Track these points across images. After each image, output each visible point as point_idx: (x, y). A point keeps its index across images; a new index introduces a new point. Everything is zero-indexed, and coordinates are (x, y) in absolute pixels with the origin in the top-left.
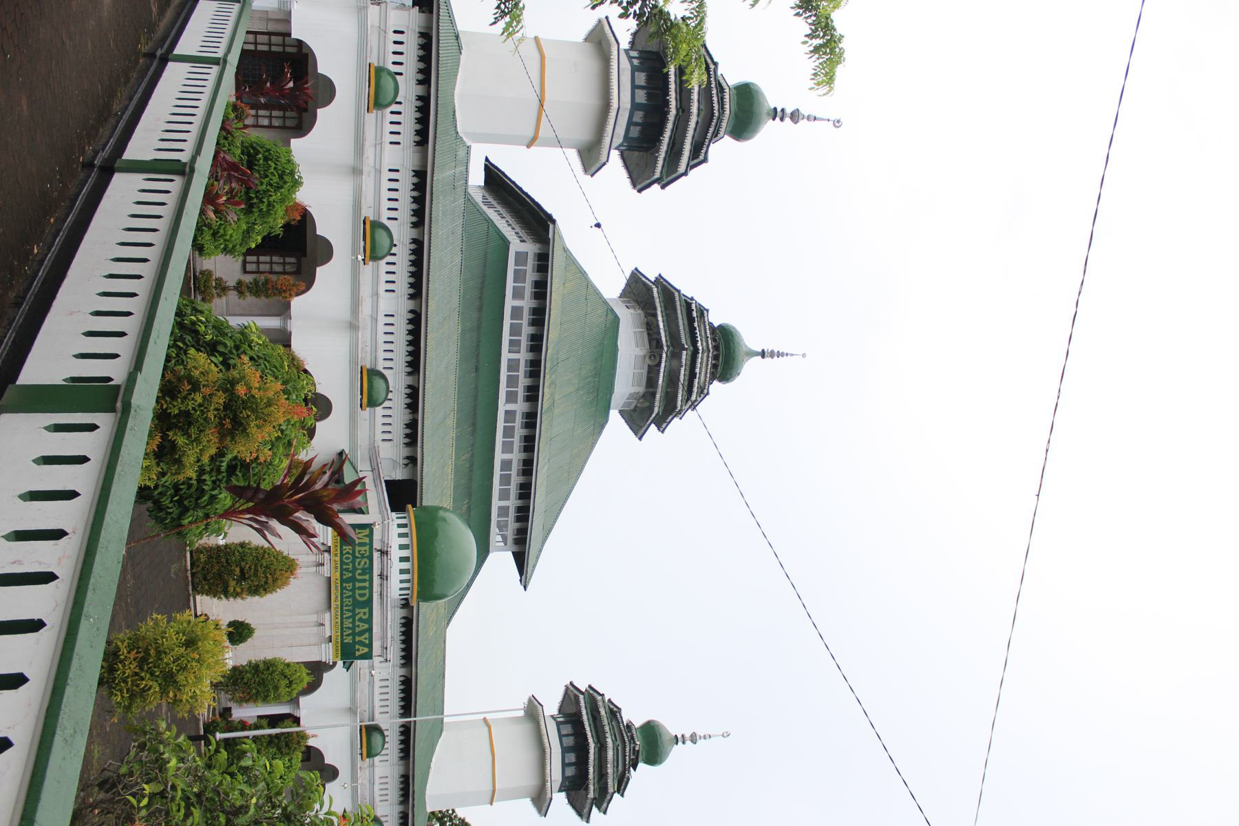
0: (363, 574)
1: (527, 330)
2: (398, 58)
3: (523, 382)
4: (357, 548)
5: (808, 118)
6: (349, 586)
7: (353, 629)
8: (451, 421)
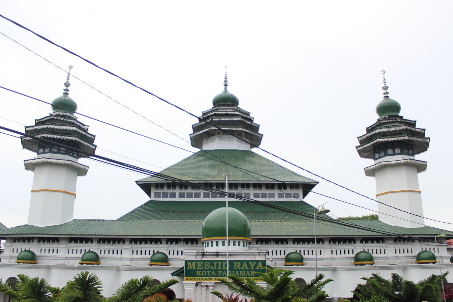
0: (213, 265)
2: (148, 252)
3: (165, 190)
4: (198, 268)
5: (385, 83)
7: (246, 271)
8: (166, 222)
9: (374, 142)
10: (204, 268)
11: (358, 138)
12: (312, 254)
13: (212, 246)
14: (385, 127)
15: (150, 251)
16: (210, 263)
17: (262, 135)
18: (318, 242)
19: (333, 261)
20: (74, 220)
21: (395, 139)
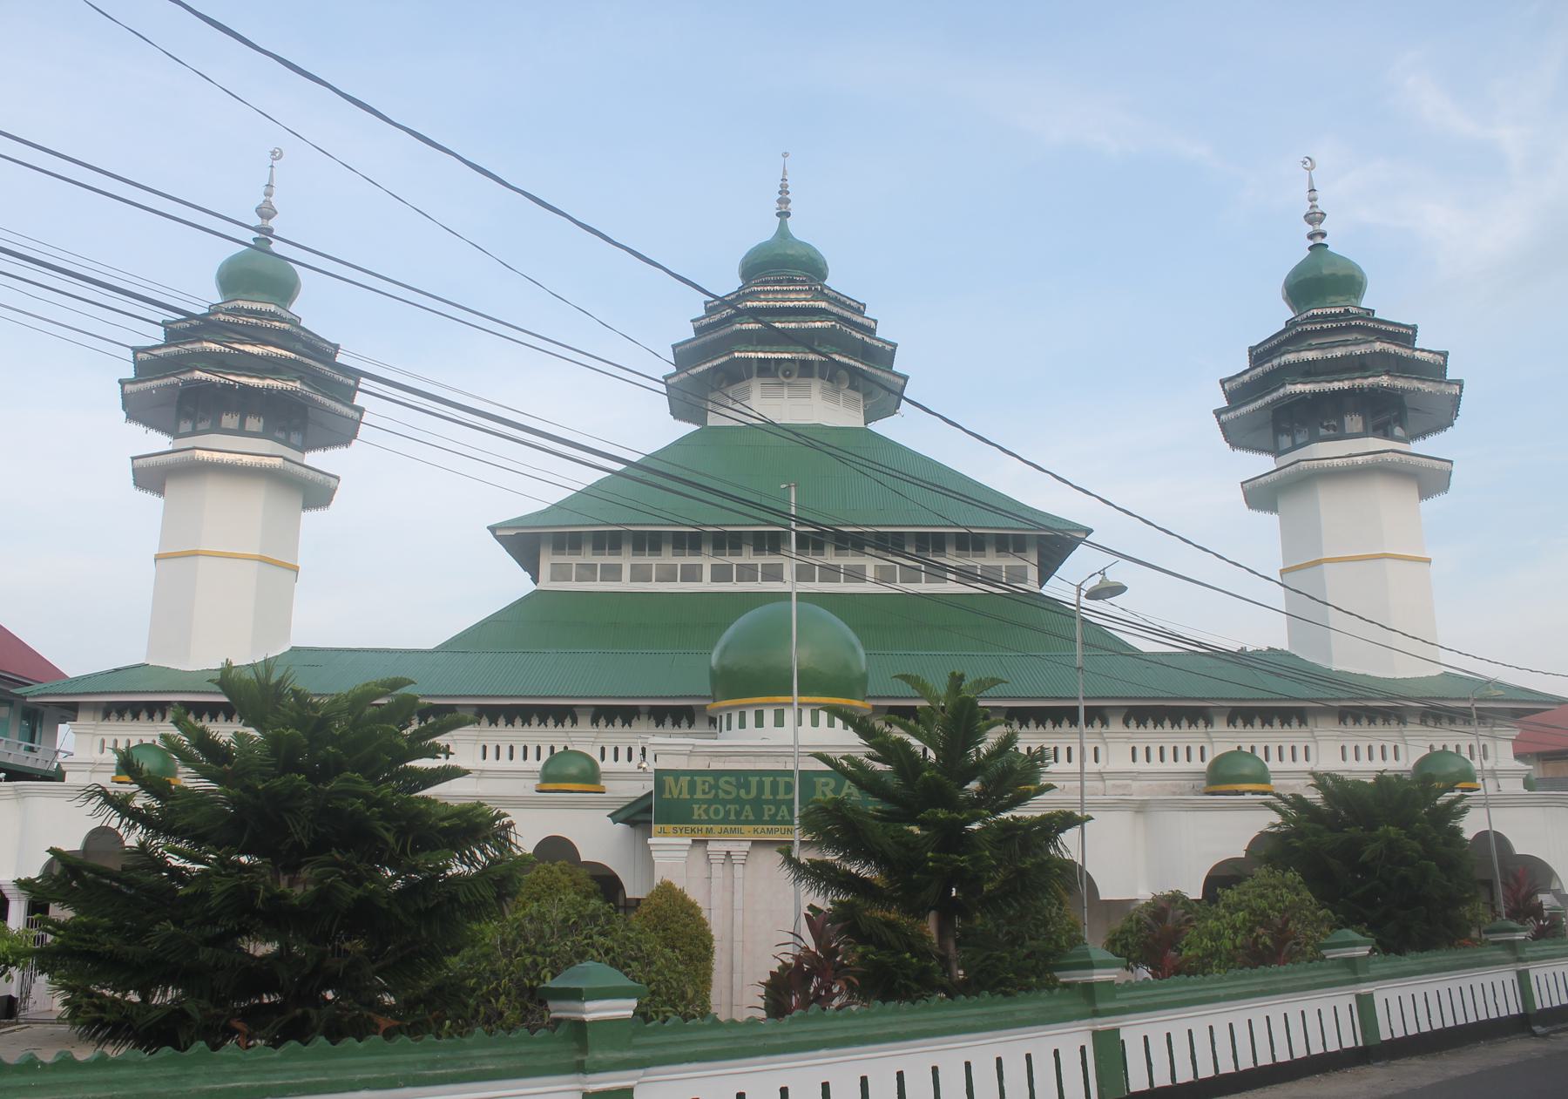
0: (747, 787)
2: (532, 753)
3: (748, 557)
4: (699, 795)
6: (768, 810)
9: (1275, 395)
10: (716, 795)
11: (1222, 382)
12: (1069, 760)
15: (539, 748)
16: (738, 780)
17: (906, 378)
18: (1089, 722)
20: (293, 649)
21: (1346, 385)
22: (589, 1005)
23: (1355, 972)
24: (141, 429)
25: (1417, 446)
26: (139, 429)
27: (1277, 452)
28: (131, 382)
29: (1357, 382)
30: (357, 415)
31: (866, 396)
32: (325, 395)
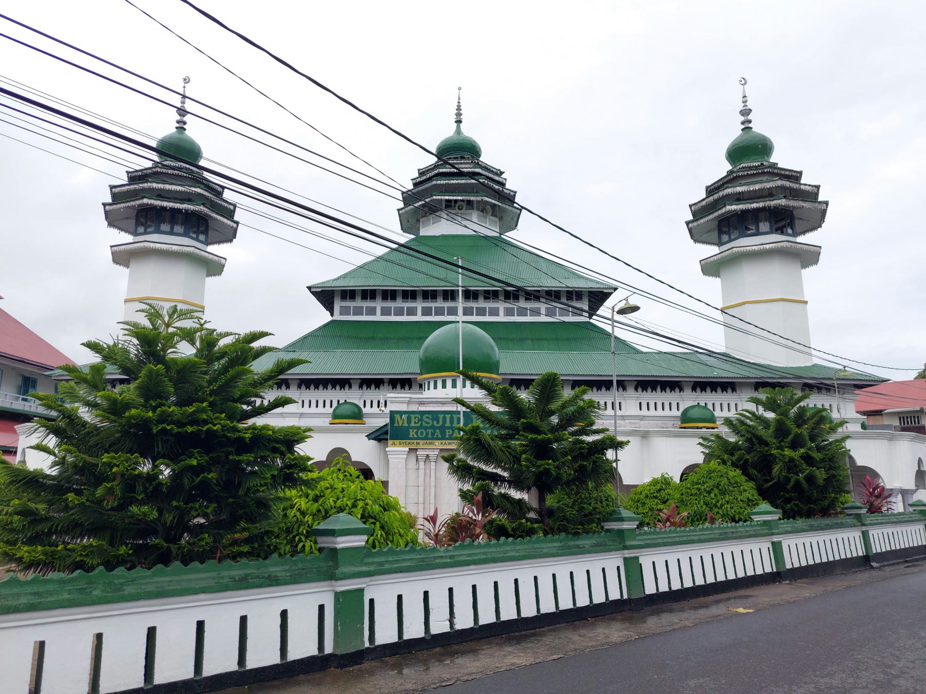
1: (399, 303)
2: (328, 404)
4: (413, 424)
5: (745, 102)
9: (720, 212)
11: (690, 206)
13: (435, 387)
14: (741, 185)
19: (642, 422)
21: (761, 205)
22: (339, 539)
23: (770, 529)
24: (116, 231)
25: (801, 239)
26: (115, 231)
27: (720, 244)
28: (110, 204)
29: (767, 203)
30: (235, 225)
31: (501, 219)
32: (217, 213)
